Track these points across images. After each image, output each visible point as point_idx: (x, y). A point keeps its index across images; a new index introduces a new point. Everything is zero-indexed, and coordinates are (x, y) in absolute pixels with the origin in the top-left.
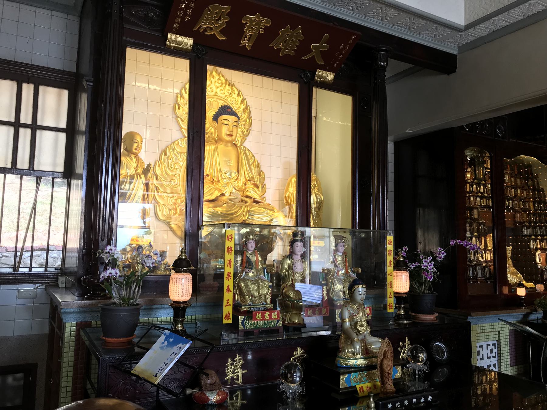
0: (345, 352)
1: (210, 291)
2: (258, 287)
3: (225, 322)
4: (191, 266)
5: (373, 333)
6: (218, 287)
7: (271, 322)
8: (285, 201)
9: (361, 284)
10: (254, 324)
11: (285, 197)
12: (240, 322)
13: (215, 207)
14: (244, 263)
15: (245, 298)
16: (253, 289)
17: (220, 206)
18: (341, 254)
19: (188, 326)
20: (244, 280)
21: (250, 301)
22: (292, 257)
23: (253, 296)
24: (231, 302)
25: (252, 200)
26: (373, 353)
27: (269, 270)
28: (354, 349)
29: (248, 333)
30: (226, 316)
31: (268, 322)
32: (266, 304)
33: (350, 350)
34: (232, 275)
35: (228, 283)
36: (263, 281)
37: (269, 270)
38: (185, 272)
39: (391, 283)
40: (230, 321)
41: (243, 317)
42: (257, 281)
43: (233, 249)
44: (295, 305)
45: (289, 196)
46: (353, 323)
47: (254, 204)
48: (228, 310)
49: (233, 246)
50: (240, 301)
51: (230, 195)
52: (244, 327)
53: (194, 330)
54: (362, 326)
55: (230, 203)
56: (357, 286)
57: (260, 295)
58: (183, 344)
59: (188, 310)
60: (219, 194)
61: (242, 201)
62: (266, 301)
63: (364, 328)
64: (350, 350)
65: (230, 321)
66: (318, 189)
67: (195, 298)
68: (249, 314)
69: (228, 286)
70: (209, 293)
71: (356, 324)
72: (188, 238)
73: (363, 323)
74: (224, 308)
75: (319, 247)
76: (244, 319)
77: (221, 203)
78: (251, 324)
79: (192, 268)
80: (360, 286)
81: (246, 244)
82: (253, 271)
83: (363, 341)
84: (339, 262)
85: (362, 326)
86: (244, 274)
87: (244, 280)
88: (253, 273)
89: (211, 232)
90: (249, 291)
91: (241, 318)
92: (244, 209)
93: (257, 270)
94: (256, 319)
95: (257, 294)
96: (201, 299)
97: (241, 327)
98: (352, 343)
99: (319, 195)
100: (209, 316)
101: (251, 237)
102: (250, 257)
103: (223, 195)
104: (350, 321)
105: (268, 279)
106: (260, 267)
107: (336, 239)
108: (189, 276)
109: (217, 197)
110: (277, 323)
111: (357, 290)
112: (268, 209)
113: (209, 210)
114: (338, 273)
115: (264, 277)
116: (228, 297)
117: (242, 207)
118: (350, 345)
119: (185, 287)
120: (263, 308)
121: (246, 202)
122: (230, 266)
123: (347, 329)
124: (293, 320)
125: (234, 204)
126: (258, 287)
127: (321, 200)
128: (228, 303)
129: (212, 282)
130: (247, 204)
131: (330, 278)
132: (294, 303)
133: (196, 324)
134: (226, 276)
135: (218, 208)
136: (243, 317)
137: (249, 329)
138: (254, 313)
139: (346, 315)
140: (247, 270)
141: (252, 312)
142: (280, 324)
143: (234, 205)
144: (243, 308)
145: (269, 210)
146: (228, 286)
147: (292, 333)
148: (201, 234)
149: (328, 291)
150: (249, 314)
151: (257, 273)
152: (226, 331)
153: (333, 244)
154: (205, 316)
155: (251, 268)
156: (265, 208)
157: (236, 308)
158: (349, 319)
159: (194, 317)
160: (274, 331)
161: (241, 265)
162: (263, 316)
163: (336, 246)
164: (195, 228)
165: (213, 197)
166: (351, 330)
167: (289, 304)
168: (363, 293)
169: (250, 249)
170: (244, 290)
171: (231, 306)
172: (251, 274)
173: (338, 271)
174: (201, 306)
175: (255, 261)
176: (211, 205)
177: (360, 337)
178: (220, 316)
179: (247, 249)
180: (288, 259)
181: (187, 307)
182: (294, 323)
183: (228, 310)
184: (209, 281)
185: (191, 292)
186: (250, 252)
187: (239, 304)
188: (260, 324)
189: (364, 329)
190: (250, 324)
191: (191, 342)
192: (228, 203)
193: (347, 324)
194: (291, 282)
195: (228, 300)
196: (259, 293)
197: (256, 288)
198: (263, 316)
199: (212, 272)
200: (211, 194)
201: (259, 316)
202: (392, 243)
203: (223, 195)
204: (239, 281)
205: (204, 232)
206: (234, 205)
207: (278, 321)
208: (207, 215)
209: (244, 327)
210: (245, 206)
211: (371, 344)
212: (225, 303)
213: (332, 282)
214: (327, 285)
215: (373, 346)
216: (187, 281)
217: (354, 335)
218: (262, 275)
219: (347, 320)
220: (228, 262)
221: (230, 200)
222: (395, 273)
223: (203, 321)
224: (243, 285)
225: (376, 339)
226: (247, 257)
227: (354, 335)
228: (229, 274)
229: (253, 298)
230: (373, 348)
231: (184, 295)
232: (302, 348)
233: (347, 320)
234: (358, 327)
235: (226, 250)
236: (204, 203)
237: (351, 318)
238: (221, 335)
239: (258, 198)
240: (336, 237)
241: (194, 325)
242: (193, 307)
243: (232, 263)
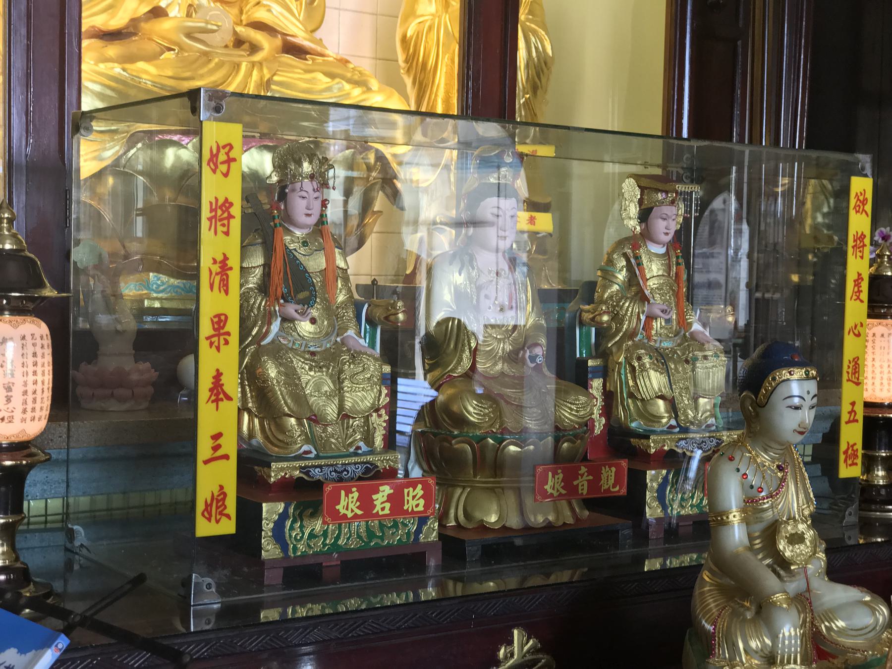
0: (733, 647)
1: (122, 400)
2: (338, 382)
3: (204, 528)
4: (42, 285)
5: (837, 573)
6: (154, 384)
7: (395, 525)
8: (401, 57)
9: (800, 365)
10: (325, 534)
11: (404, 40)
12: (267, 526)
13: (128, 59)
14: (277, 278)
15: (282, 428)
16: (318, 387)
17: (150, 58)
18: (662, 250)
19: (34, 541)
20: (277, 352)
21: (307, 441)
22: (472, 259)
23: (316, 419)
24: (230, 446)
25: (278, 42)
26: (845, 650)
27: (379, 313)
28: (774, 637)
29: (303, 575)
30: (208, 506)
31: (382, 526)
32: (372, 452)
33: (754, 644)
34: (233, 326)
35: (217, 361)
36: (355, 356)
37: (379, 313)
38: (18, 310)
39: (856, 364)
40: (228, 527)
41: (281, 507)
42: (330, 358)
43: (236, 211)
44: (490, 456)
45: (418, 35)
46: (758, 528)
47: (288, 58)
48: (215, 478)
49: (236, 199)
50: (259, 438)
51: (189, 15)
52: (284, 547)
53: (57, 558)
54: (796, 539)
55: (191, 49)
56: (785, 374)
57: (344, 416)
58: (22, 651)
59: (35, 480)
60: (145, 9)
61: (239, 42)
62: (368, 439)
63: (803, 549)
64: (754, 644)
65: (228, 527)
66: (531, 12)
67: (61, 428)
68: (307, 495)
69: (218, 375)
70: (113, 406)
71: (771, 532)
72: (21, 180)
73: (802, 527)
74: (201, 468)
75: (533, 235)
76: (283, 516)
77: (151, 47)
78: (312, 536)
79: (49, 292)
80: (799, 373)
81: (283, 196)
82: (314, 313)
83: (802, 600)
84: (652, 283)
85: (796, 539)
86: (275, 327)
87: (277, 352)
88: (313, 321)
89: (116, 163)
90: (300, 398)
91: (271, 511)
92: (249, 74)
93: (330, 311)
94: (336, 516)
95: (331, 411)
96: (85, 430)
97: (269, 550)
98: (764, 613)
99: (535, 33)
100: (117, 501)
101: (306, 167)
102: (301, 252)
103: (157, 13)
104: (746, 521)
105: (372, 345)
106: (341, 298)
107: (642, 189)
108: (37, 330)
109: (135, 22)
110: (419, 531)
111: (782, 391)
112: (343, 78)
113: (102, 67)
114: (647, 327)
115: (357, 338)
116: (220, 423)
117: (237, 67)
118: (753, 620)
119: (19, 380)
120: (359, 471)
121: (254, 48)
122: (225, 287)
123: (737, 555)
124: (478, 515)
125: (205, 54)
126: (338, 382)
127: (542, 54)
128: (216, 448)
129: (128, 364)
130: (257, 57)
131: (619, 344)
132: (484, 448)
133: (71, 535)
134: (206, 328)
135: (141, 65)
136: (281, 507)
137: (304, 556)
138: (328, 489)
139: (732, 495)
140: (291, 309)
141: (318, 485)
142: (431, 533)
143: (206, 56)
144: (277, 472)
145: (349, 81)
146: (218, 375)
147: (477, 569)
148: (78, 170)
149: (609, 396)
150: (307, 495)
151: (331, 325)
152: (211, 568)
153: (633, 210)
154: (101, 502)
155: (308, 302)
156: (332, 76)
157: (251, 465)
158: (743, 510)
159: (55, 505)
160: (404, 563)
161: (264, 288)
162: (366, 503)
163: (645, 216)
164: (50, 139)
165: (118, 21)
166: (749, 555)
167: (464, 451)
168: (809, 401)
169: (302, 219)
170: (280, 392)
171: (231, 466)
172: (305, 327)
173: (651, 318)
174: (83, 461)
175: (323, 272)
176: (113, 50)
177: (794, 586)
178: (181, 495)
179: (288, 219)
180: (455, 268)
181: (30, 467)
182: (483, 527)
183: (215, 478)
184: (116, 359)
185: (47, 403)
186: (298, 233)
187: (258, 451)
188: (350, 538)
189: (805, 551)
190: (310, 536)
191: (63, 642)
192: (181, 49)
193: (736, 533)
194: (466, 363)
195: (217, 436)
196: (341, 407)
197: (328, 386)
198: (366, 503)
199: (130, 324)
200: (110, 7)
201: (348, 504)
202: (868, 207)
203: (157, 13)
204: (256, 357)
205: (91, 155)
206: (206, 56)
207: (423, 521)
208: (97, 88)
209: (284, 547)
210: (253, 64)
211: (830, 615)
212: (204, 449)
213: (628, 361)
214: (604, 373)
215: (841, 624)
216: (30, 350)
217: (770, 581)
218: (351, 332)
219: (735, 517)
220: (216, 268)
221: (189, 36)
222: (878, 327)
223: (95, 520)
224: (272, 372)
225: (851, 593)
226: (288, 253)
227: (770, 581)
228: (220, 322)
229: (318, 429)
230: (841, 631)
231: (18, 415)
232: (530, 631)
233: (735, 517)
234: (782, 545)
235: (205, 213)
236: (85, 43)
237: (750, 505)
238: (186, 583)
239: (301, 38)
240: (645, 183)
241: (60, 538)
242: (57, 462)
243: (234, 277)
